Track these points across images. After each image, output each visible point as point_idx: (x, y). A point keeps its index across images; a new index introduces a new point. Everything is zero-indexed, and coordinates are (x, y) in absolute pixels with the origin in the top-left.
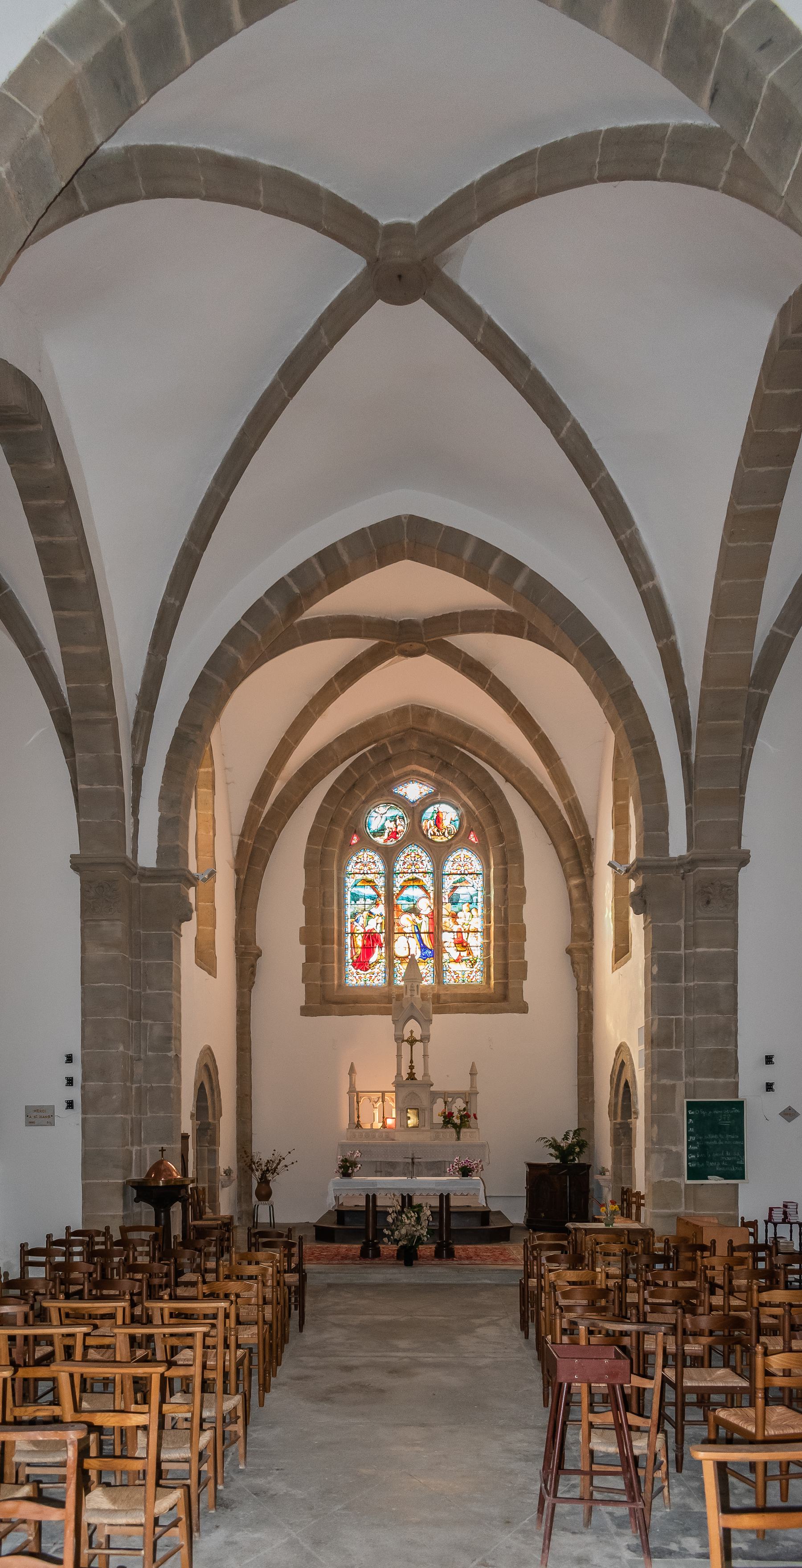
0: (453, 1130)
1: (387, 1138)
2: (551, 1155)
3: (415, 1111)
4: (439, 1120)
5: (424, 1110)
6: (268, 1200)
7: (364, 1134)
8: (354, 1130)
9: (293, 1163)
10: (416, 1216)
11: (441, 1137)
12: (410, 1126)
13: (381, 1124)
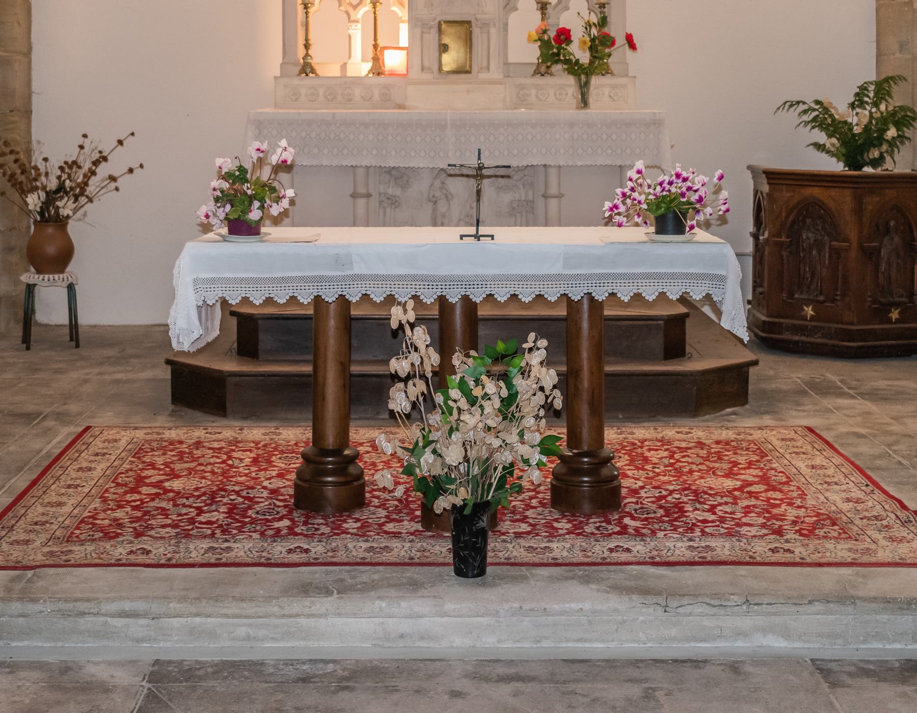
0: (571, 80)
1: (386, 100)
2: (819, 147)
3: (462, 30)
4: (532, 54)
5: (486, 25)
6: (62, 272)
7: (321, 91)
8: (296, 81)
9: (131, 171)
10: (505, 393)
11: (533, 99)
12: (446, 68)
13: (368, 66)
